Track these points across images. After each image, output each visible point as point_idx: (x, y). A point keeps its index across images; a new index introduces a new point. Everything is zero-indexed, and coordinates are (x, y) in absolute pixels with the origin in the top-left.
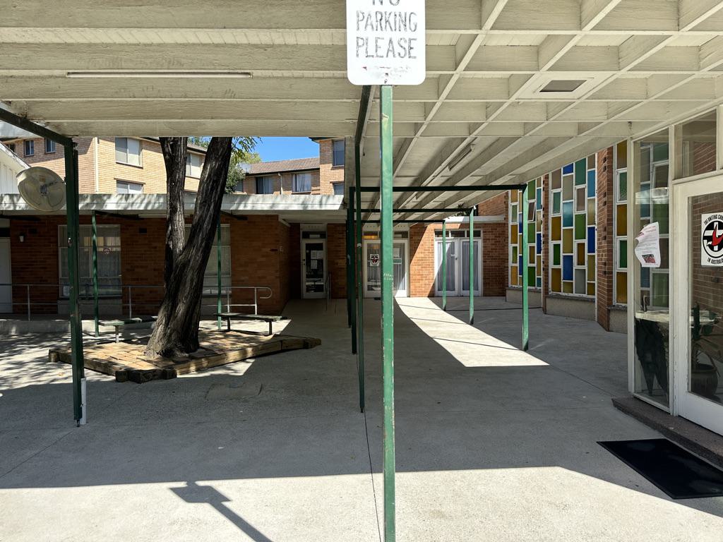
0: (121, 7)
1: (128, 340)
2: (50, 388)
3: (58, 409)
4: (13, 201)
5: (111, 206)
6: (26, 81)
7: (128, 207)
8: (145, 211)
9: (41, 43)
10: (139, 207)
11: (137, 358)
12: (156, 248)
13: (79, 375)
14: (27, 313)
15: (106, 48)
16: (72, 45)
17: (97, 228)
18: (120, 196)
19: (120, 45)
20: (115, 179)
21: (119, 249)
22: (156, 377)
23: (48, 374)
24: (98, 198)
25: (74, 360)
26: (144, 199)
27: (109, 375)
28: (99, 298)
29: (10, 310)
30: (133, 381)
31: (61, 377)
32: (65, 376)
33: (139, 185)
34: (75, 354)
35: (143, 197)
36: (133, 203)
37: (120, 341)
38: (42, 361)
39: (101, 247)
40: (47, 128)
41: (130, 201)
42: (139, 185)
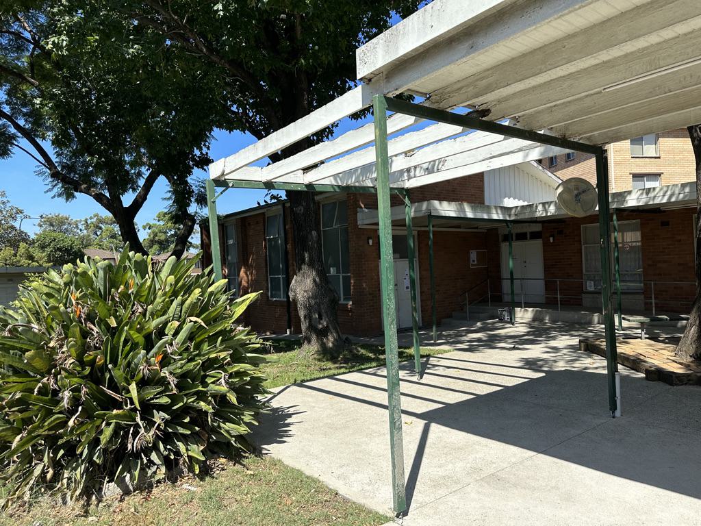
0: (664, 8)
1: (654, 338)
2: (582, 375)
3: (593, 397)
4: (545, 208)
5: (632, 202)
6: (566, 106)
7: (649, 202)
8: (669, 203)
9: (581, 69)
10: (662, 200)
11: (667, 359)
12: (680, 240)
13: (613, 369)
14: (557, 304)
15: (643, 52)
16: (609, 61)
17: (618, 225)
18: (641, 192)
19: (658, 44)
20: (630, 174)
21: (639, 244)
22: (691, 382)
23: (580, 362)
24: (622, 196)
25: (609, 355)
26: (666, 192)
27: (638, 372)
28: (622, 293)
29: (542, 300)
30: (667, 383)
31: (591, 366)
32: (595, 366)
33: (656, 176)
34: (609, 349)
35: (665, 189)
36: (654, 197)
37: (646, 338)
38: (572, 347)
39: (621, 243)
40: (580, 142)
41: (652, 195)
42: (656, 176)
